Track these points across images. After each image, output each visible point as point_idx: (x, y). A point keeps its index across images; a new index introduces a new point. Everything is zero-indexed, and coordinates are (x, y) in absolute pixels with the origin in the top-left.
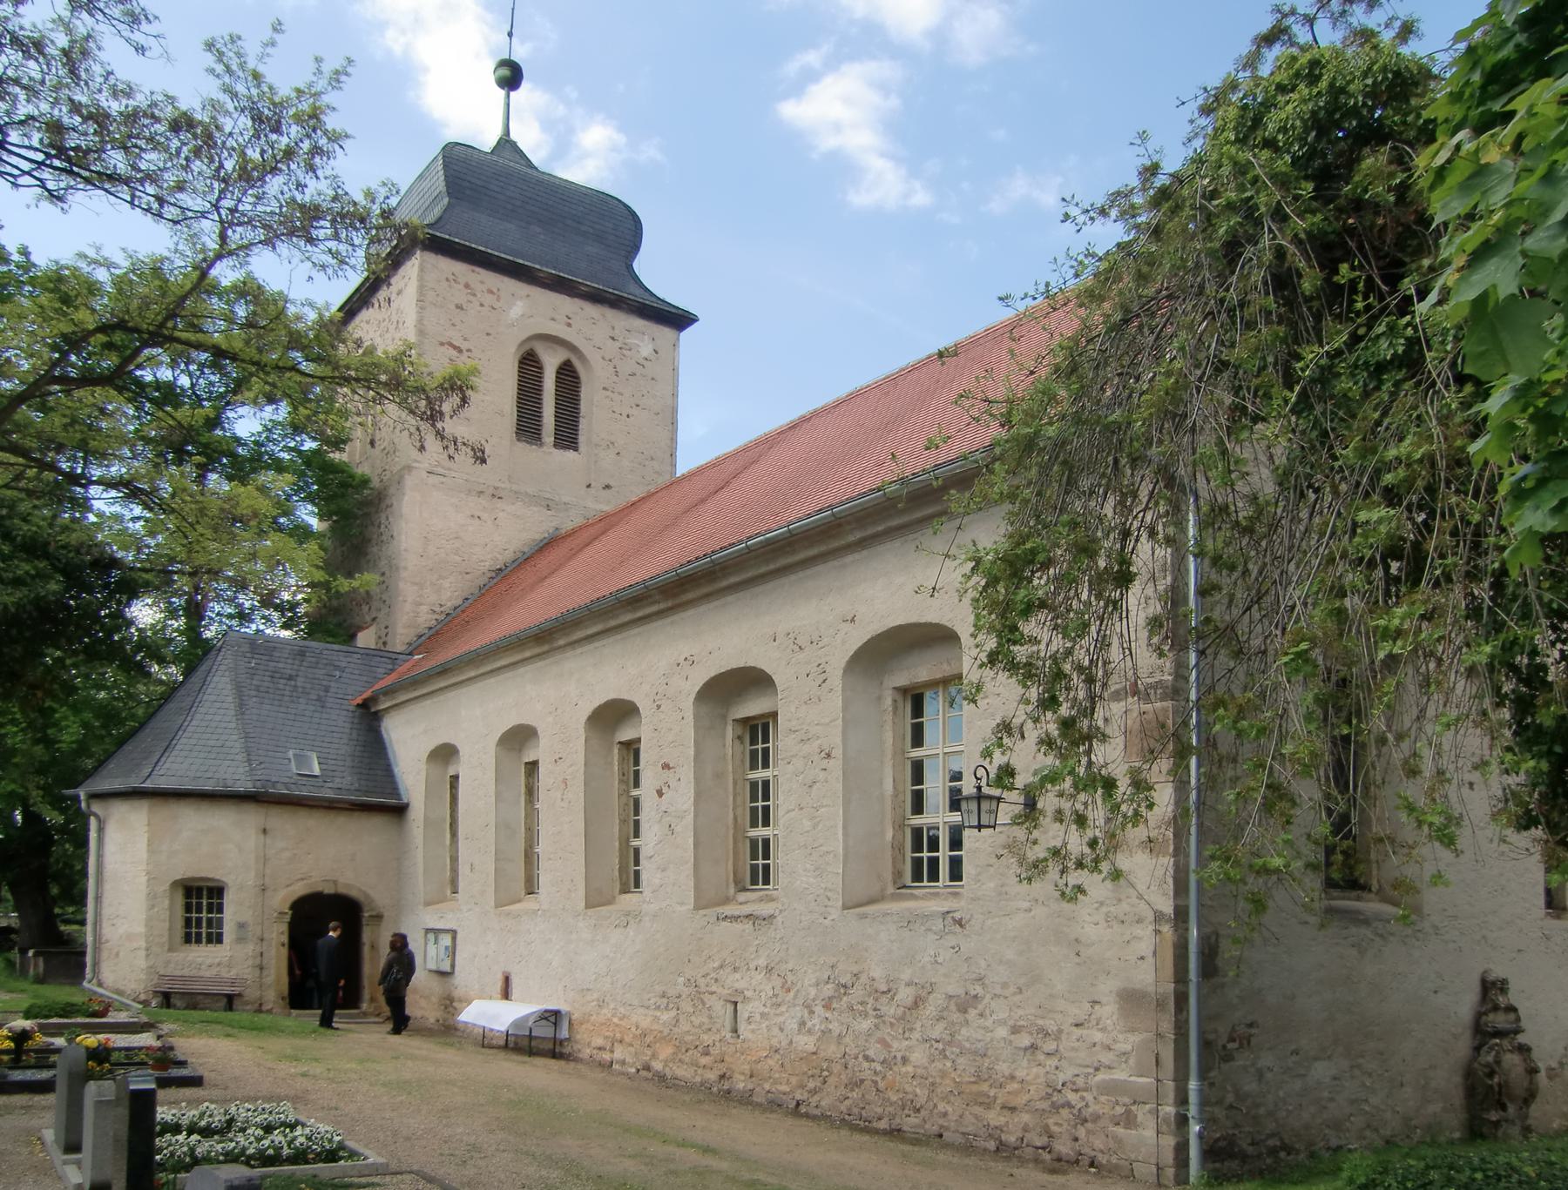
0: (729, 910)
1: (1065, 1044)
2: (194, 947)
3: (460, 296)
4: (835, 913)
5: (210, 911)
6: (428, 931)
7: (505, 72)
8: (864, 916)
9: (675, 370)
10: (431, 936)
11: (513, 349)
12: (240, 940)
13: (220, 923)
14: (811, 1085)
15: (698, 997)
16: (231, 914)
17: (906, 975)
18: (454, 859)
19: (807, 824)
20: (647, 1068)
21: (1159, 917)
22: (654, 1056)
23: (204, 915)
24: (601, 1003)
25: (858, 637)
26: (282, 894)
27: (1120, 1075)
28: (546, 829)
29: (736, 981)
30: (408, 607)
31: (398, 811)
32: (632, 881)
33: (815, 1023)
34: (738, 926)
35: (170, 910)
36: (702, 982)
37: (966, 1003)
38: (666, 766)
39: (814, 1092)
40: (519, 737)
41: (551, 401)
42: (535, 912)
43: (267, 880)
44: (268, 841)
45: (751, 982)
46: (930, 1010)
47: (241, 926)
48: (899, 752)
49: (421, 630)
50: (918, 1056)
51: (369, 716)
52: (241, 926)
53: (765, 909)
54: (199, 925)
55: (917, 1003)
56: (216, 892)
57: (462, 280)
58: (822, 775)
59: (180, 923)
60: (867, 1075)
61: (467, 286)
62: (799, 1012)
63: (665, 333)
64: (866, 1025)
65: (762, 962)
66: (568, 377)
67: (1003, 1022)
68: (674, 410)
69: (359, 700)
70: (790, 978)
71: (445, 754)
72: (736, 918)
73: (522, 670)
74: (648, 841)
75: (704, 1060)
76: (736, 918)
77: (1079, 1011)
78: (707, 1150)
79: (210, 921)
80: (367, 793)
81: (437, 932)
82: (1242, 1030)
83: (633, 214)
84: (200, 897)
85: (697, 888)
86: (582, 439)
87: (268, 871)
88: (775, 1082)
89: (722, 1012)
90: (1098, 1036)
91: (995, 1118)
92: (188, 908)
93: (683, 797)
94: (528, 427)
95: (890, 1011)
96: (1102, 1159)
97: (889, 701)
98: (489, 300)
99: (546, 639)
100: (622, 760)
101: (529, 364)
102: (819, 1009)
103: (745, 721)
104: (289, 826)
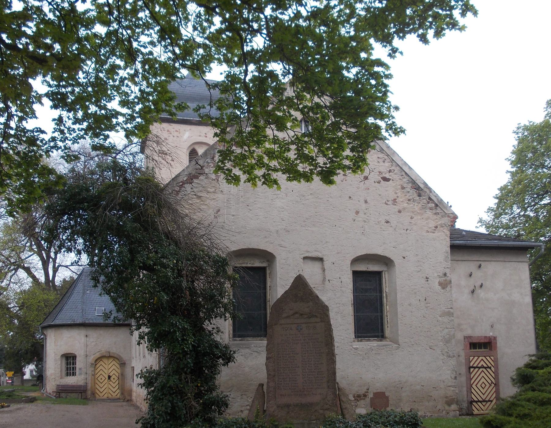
5: (73, 365)
16: (80, 364)
26: (92, 357)
43: (88, 353)
44: (88, 339)
47: (80, 369)
54: (70, 370)
56: (74, 357)
57: (166, 130)
61: (168, 131)
78: (505, 261)
79: (73, 368)
87: (88, 350)
98: (176, 134)
104: (94, 334)
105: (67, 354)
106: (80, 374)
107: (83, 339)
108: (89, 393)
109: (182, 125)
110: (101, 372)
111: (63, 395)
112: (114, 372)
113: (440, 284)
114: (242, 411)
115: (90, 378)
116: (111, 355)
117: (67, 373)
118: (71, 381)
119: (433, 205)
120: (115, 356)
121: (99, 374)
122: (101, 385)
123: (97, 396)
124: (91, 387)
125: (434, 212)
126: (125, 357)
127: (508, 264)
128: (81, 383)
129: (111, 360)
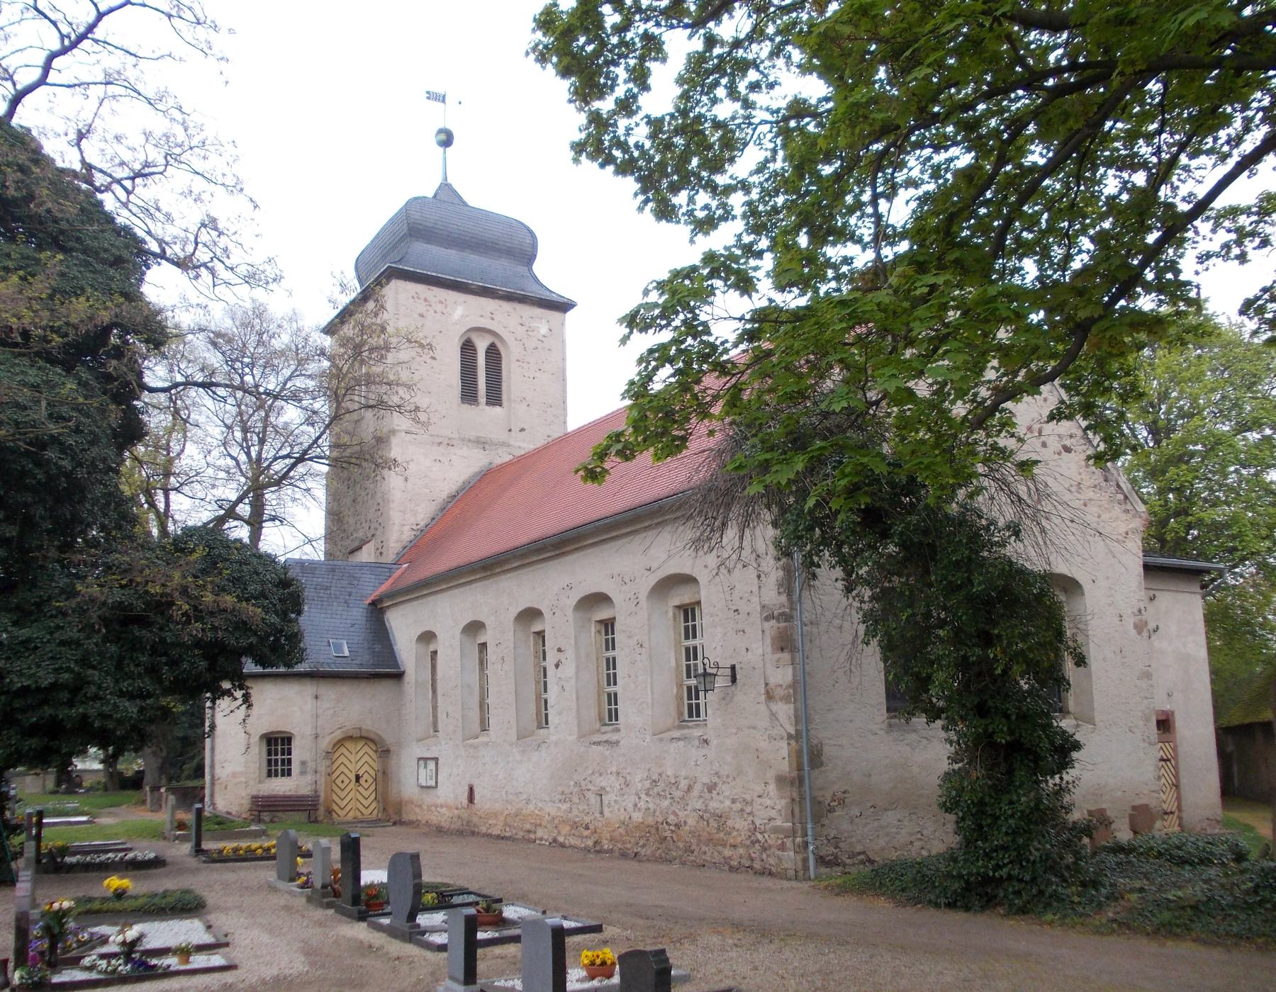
0: (597, 738)
1: (756, 806)
2: (273, 779)
3: (421, 307)
4: (648, 739)
5: (283, 754)
6: (420, 759)
7: (443, 137)
8: (661, 740)
9: (563, 341)
10: (422, 763)
11: (457, 339)
12: (303, 773)
13: (290, 761)
14: (641, 843)
15: (582, 793)
16: (298, 753)
17: (683, 773)
18: (435, 708)
19: (632, 686)
20: (555, 840)
21: (790, 736)
22: (559, 833)
23: (279, 757)
24: (528, 801)
25: (653, 580)
26: (327, 740)
27: (779, 823)
28: (493, 689)
29: (602, 782)
30: (396, 528)
31: (398, 676)
32: (543, 721)
33: (642, 804)
34: (600, 748)
35: (258, 753)
36: (583, 783)
37: (711, 788)
38: (559, 650)
39: (644, 846)
40: (474, 627)
41: (482, 373)
42: (487, 744)
45: (609, 782)
46: (695, 793)
47: (303, 763)
48: (678, 643)
49: (405, 543)
50: (691, 822)
51: (377, 610)
52: (303, 763)
53: (614, 737)
54: (276, 764)
55: (690, 788)
57: (422, 297)
58: (638, 657)
59: (265, 764)
60: (668, 834)
61: (426, 300)
62: (633, 798)
63: (555, 315)
64: (666, 803)
65: (614, 769)
66: (494, 354)
67: (728, 797)
68: (564, 371)
69: (369, 601)
70: (629, 778)
71: (427, 637)
72: (599, 743)
73: (474, 585)
74: (552, 695)
75: (586, 833)
76: (599, 743)
77: (759, 788)
79: (283, 760)
80: (377, 666)
81: (426, 759)
82: (839, 795)
83: (531, 232)
84: (276, 744)
85: (579, 725)
86: (504, 397)
88: (624, 843)
89: (593, 799)
90: (768, 802)
91: (727, 852)
92: (269, 754)
93: (568, 669)
94: (469, 394)
95: (678, 794)
96: (774, 870)
97: (671, 614)
98: (439, 308)
99: (490, 567)
100: (536, 644)
101: (468, 348)
102: (643, 796)
103: (601, 622)
104: (330, 692)
105: (272, 733)
106: (303, 773)
107: (309, 704)
108: (322, 809)
109: (451, 292)
110: (342, 768)
111: (266, 816)
112: (366, 767)
113: (1136, 626)
114: (912, 843)
115: (323, 779)
116: (364, 734)
117: (269, 771)
118: (280, 786)
119: (1122, 497)
120: (372, 736)
121: (337, 773)
122: (342, 795)
123: (334, 815)
124: (326, 798)
125: (1123, 507)
126: (389, 738)
127: (1180, 596)
128: (306, 791)
129: (361, 744)
